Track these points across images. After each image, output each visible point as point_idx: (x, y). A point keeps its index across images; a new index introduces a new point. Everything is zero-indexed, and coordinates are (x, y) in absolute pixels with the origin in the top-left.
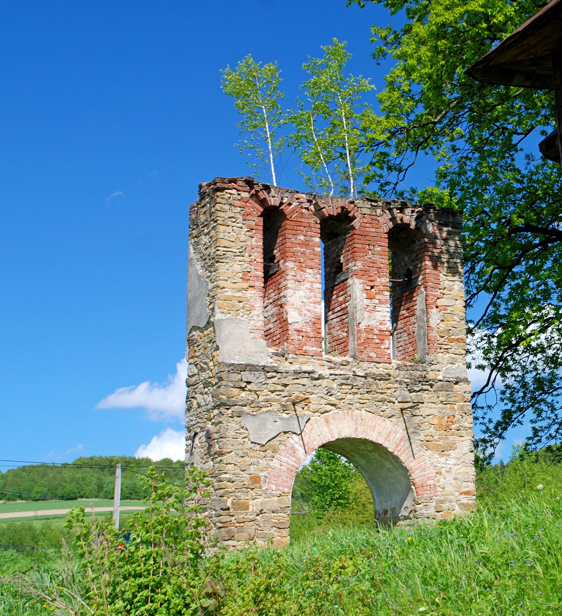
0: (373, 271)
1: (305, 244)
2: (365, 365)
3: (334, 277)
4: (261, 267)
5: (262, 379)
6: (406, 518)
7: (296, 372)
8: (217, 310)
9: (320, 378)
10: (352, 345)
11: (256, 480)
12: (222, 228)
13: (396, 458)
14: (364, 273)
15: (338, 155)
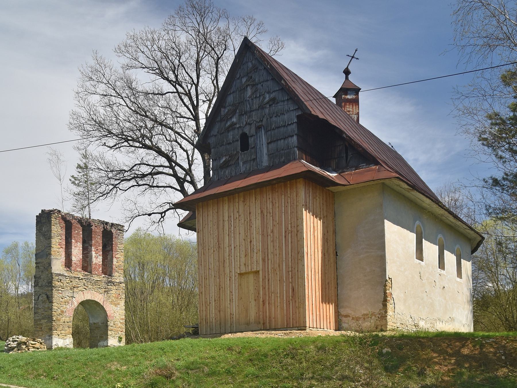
15: (111, 187)
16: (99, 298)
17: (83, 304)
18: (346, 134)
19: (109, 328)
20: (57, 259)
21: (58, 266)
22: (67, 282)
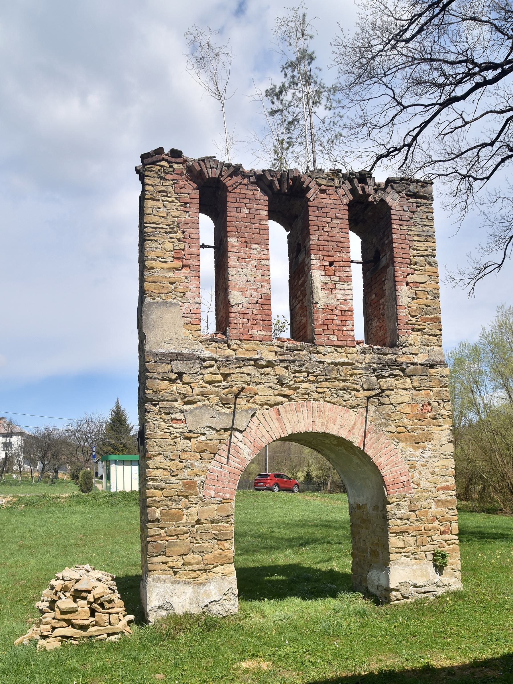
16: (344, 423)
19: (394, 524)
20: (165, 304)
22: (208, 377)
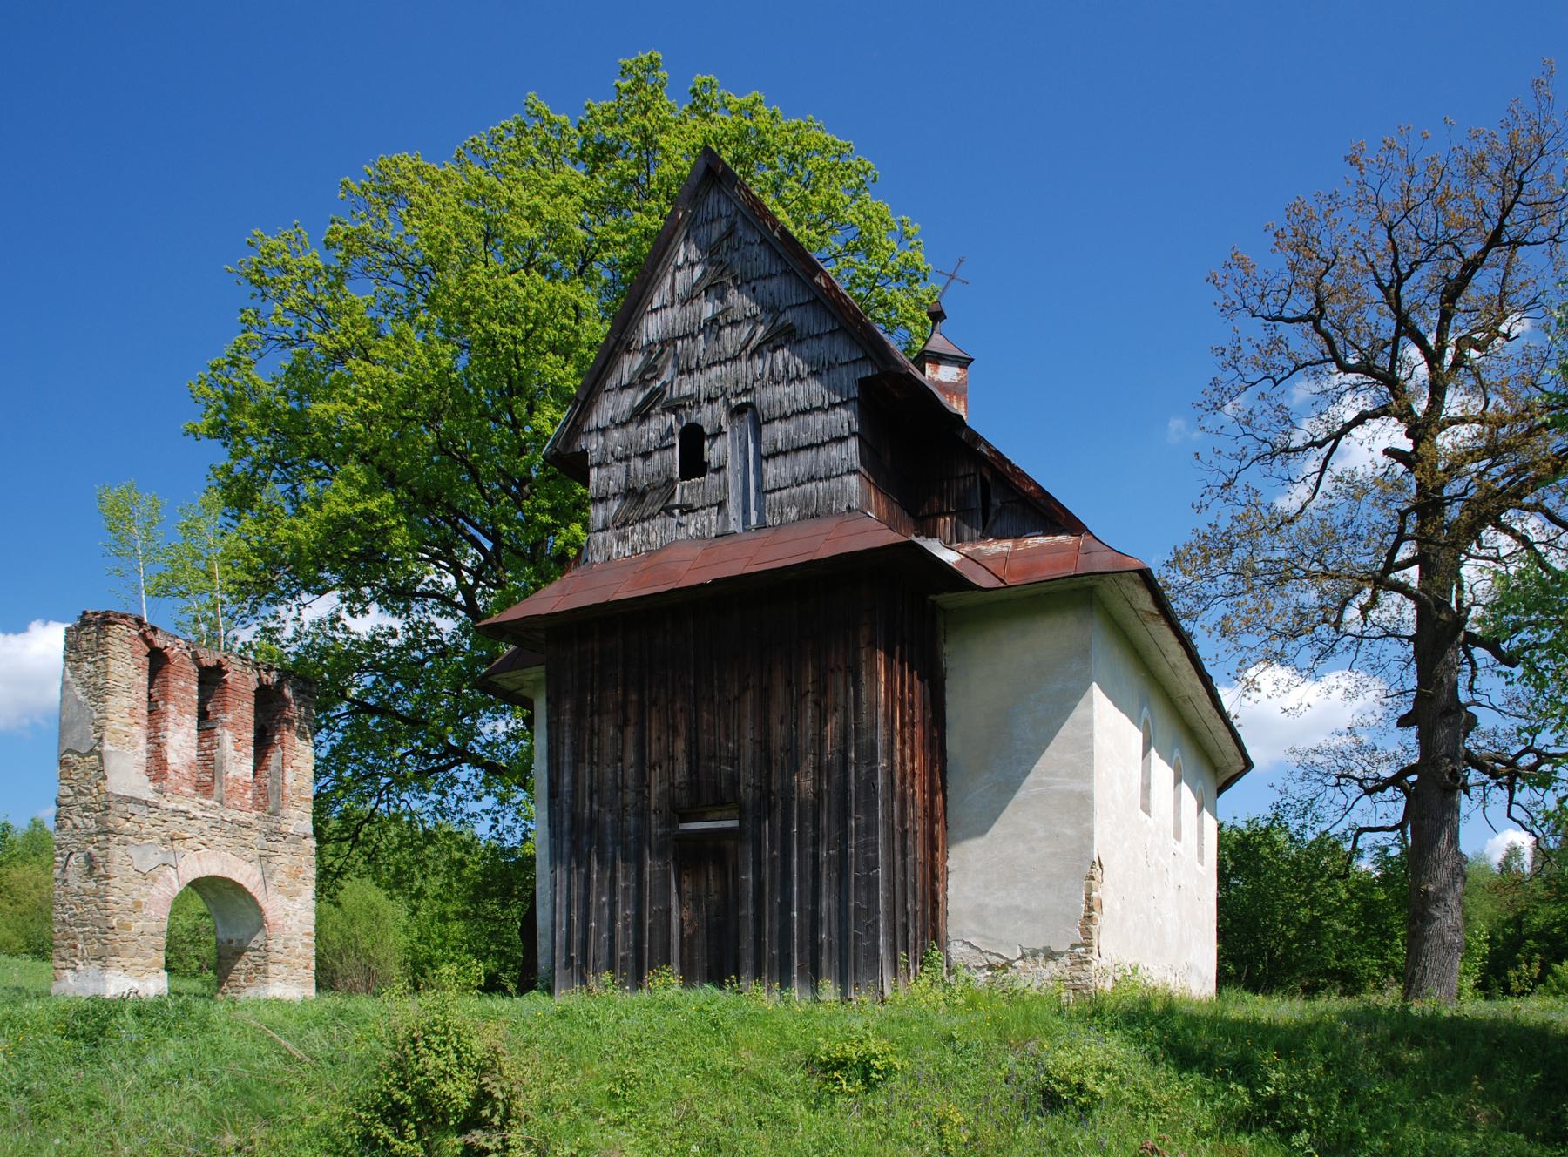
0: (241, 726)
1: (185, 690)
2: (231, 811)
3: (205, 721)
4: (146, 706)
5: (145, 812)
6: (254, 950)
7: (174, 811)
8: (106, 741)
9: (195, 818)
10: (216, 791)
11: (138, 904)
12: (112, 662)
13: (254, 899)
14: (233, 726)
16: (244, 873)
17: (201, 886)
18: (988, 445)
21: (126, 772)
